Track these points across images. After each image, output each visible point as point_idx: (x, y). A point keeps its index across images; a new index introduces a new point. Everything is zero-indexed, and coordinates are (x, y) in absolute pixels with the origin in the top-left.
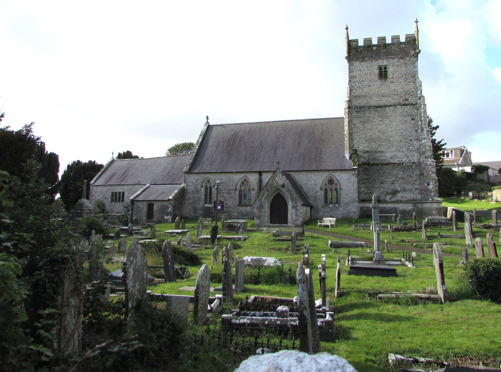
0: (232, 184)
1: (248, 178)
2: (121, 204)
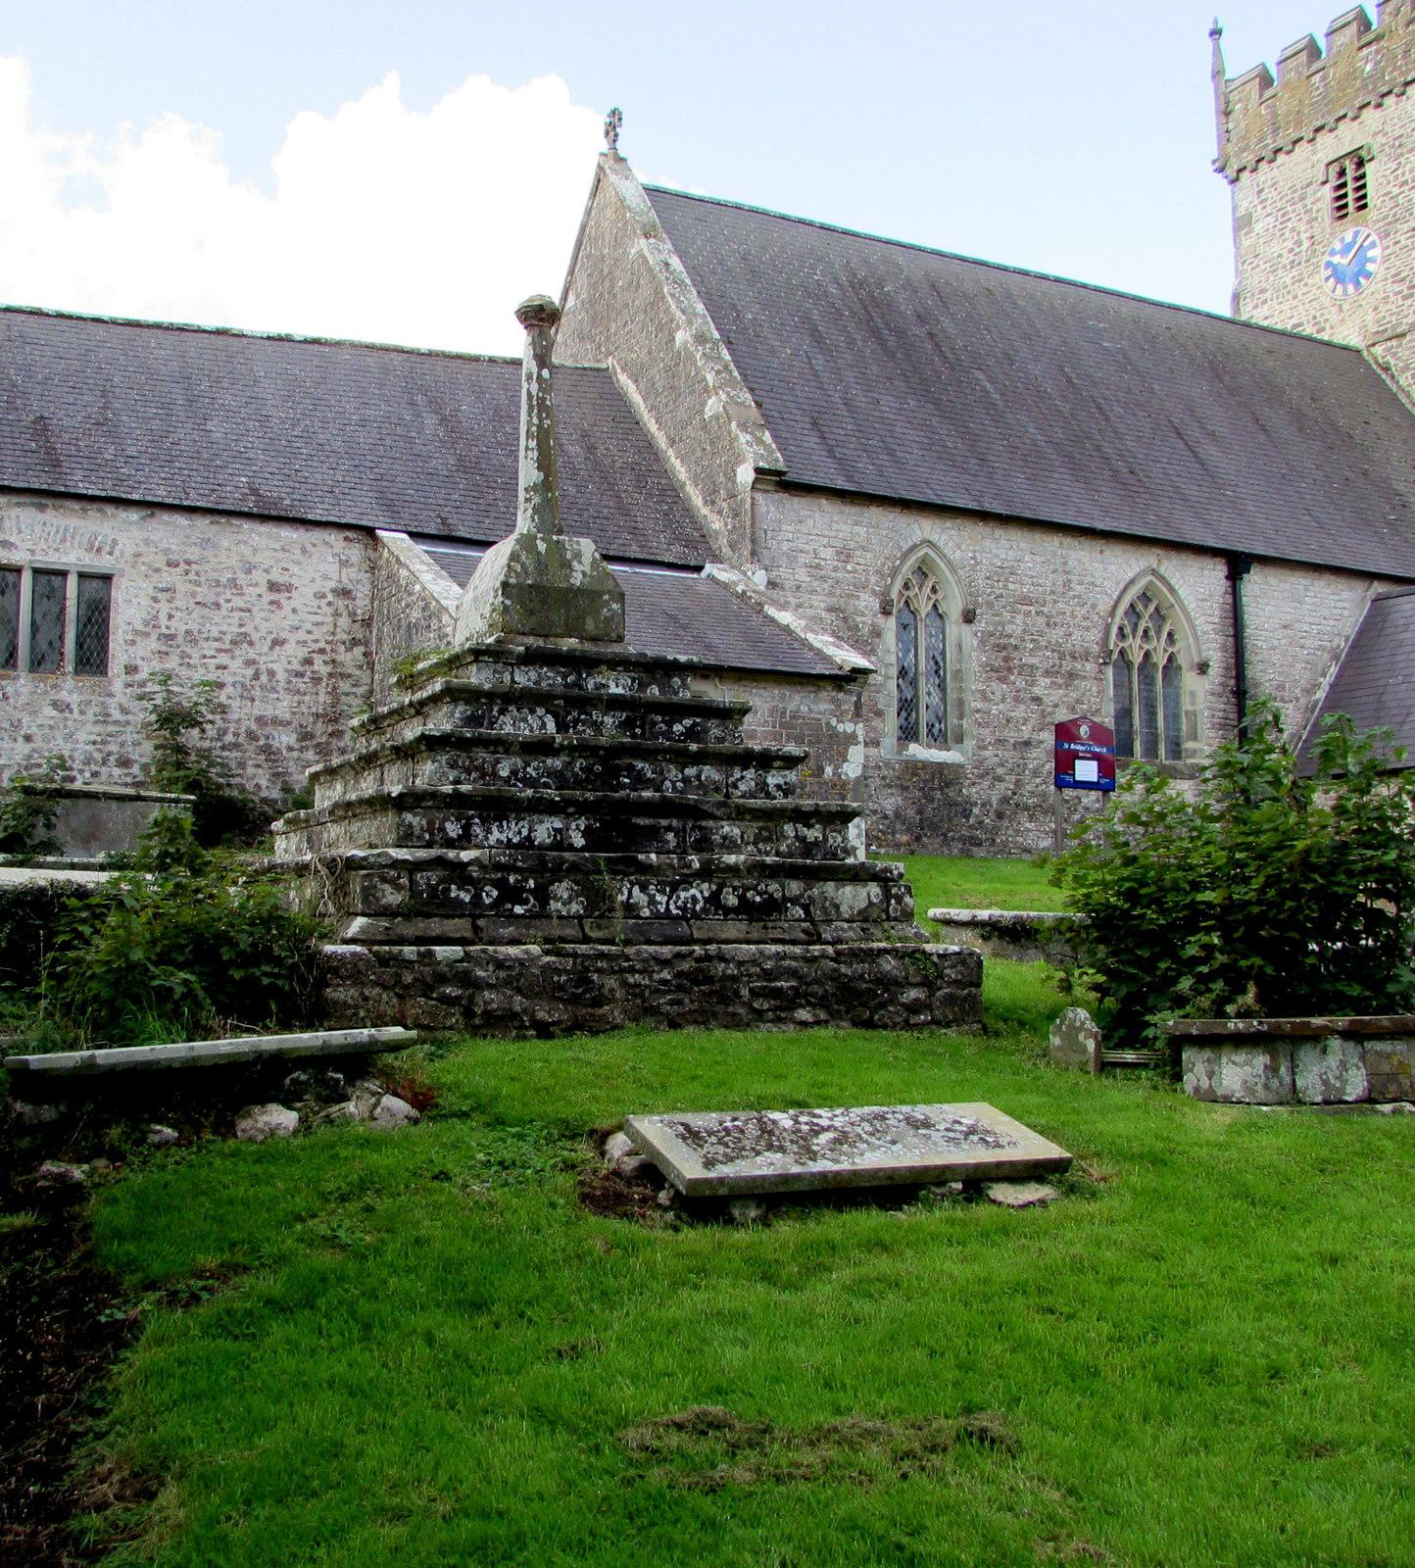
0: (1081, 612)
1: (1172, 590)
2: (71, 688)
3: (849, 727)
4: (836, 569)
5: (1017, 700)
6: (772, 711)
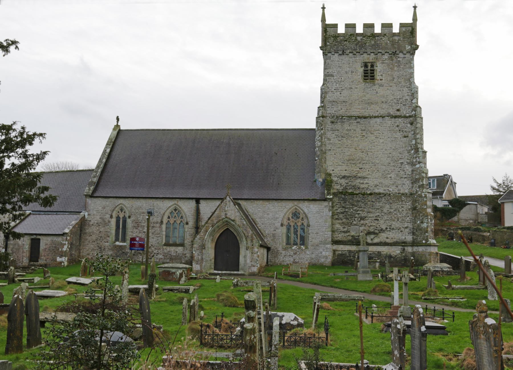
1: (180, 207)
3: (64, 242)
4: (102, 211)
5: (140, 232)
6: (51, 240)
